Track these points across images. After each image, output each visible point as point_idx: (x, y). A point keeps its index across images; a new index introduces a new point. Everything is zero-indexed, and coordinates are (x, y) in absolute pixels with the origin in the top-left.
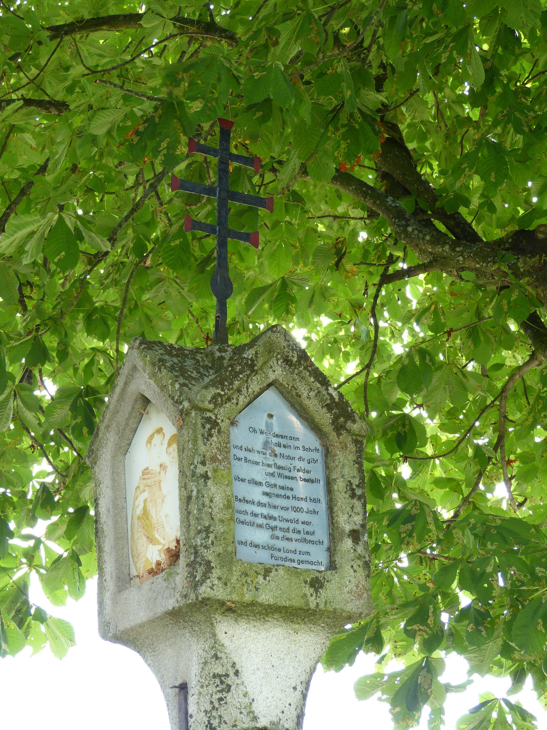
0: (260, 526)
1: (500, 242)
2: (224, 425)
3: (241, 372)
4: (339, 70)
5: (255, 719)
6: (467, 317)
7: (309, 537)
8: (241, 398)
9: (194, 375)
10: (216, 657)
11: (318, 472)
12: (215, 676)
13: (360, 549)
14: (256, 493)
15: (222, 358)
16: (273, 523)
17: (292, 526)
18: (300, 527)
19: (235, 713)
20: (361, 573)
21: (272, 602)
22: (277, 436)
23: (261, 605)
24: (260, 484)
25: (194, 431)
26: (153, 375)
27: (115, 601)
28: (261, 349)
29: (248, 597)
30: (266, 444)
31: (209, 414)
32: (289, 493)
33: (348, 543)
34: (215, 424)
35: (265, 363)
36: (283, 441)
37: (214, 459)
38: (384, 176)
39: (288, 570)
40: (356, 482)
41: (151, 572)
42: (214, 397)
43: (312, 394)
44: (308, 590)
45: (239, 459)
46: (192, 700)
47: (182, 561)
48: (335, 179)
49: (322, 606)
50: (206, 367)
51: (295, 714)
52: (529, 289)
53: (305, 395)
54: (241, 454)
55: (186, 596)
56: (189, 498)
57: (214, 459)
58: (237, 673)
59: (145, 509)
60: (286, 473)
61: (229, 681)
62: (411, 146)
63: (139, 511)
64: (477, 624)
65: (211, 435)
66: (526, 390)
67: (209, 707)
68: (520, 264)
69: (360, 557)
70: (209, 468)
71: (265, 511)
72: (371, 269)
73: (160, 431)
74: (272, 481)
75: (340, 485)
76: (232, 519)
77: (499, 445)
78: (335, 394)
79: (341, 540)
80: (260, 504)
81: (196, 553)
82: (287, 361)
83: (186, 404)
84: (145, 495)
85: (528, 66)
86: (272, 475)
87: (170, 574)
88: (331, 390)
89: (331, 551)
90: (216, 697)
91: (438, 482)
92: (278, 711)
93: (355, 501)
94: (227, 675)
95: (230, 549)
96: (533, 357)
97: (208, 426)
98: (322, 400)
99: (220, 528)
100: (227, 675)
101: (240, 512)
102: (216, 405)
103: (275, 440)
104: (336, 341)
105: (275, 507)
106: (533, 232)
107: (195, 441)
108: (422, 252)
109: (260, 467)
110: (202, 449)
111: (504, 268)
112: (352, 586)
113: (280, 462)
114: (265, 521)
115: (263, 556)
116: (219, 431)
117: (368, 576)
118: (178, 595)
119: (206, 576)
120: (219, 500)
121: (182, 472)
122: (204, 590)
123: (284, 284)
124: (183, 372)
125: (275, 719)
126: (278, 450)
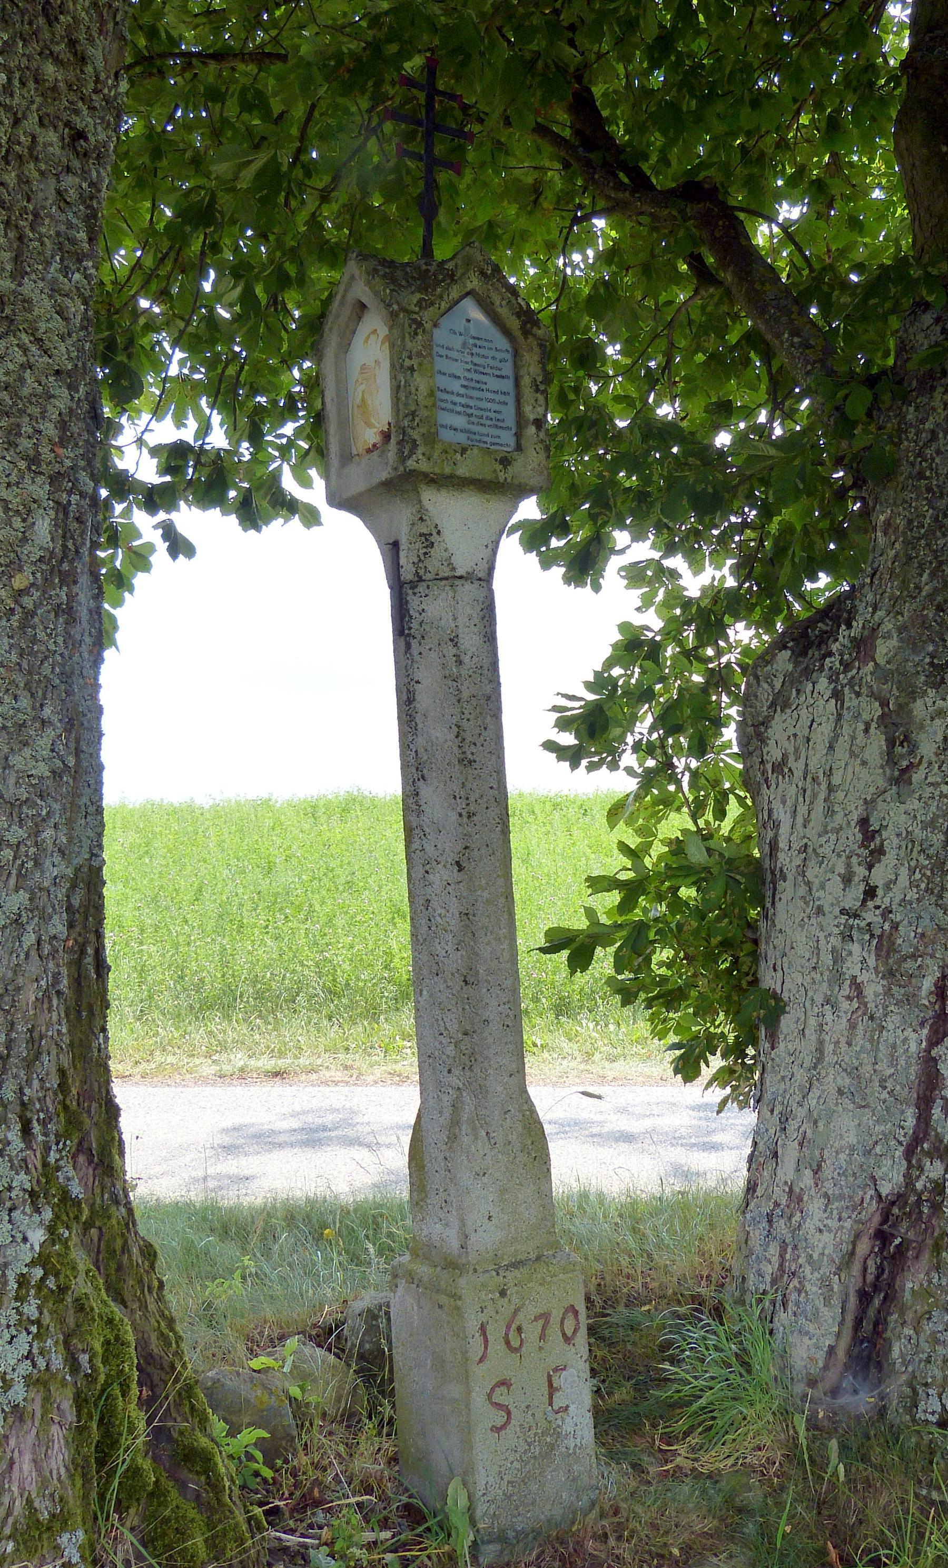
0: (459, 413)
1: (672, 191)
2: (428, 326)
3: (443, 281)
4: (535, 22)
5: (454, 569)
6: (643, 256)
7: (500, 424)
8: (443, 304)
9: (404, 283)
10: (421, 519)
11: (508, 369)
12: (421, 535)
13: (542, 435)
14: (455, 386)
15: (427, 271)
16: (469, 411)
17: (485, 414)
18: (492, 415)
19: (438, 564)
20: (543, 455)
21: (468, 475)
22: (474, 338)
23: (459, 477)
24: (459, 378)
25: (403, 330)
26: (368, 283)
27: (339, 475)
28: (460, 262)
29: (447, 471)
30: (464, 344)
31: (415, 316)
32: (484, 387)
33: (532, 429)
34: (420, 324)
35: (464, 274)
36: (479, 343)
37: (419, 354)
38: (577, 132)
39: (481, 449)
40: (540, 379)
41: (369, 451)
42: (420, 302)
43: (504, 303)
44: (499, 467)
45: (441, 356)
46: (402, 554)
47: (393, 440)
48: (534, 130)
49: (509, 480)
50: (413, 278)
51: (486, 566)
52: (694, 230)
53: (498, 303)
54: (443, 352)
55: (396, 469)
56: (398, 387)
57: (419, 354)
58: (439, 533)
59: (363, 399)
60: (481, 370)
61: (432, 539)
62: (605, 113)
63: (358, 401)
64: (640, 501)
65: (416, 334)
66: (690, 322)
67: (416, 560)
68: (688, 210)
69: (542, 441)
70: (415, 362)
71: (463, 401)
72: (564, 214)
73: (374, 332)
74: (469, 376)
75: (526, 381)
76: (434, 405)
77: (667, 366)
78: (523, 303)
79: (526, 427)
80: (458, 395)
81: (404, 433)
82: (483, 273)
83: (395, 307)
84: (363, 386)
85: (704, 45)
86: (469, 370)
87: (383, 451)
88: (520, 300)
89: (518, 436)
90: (422, 551)
91: (617, 399)
92: (473, 564)
93: (538, 395)
94: (431, 535)
95: (432, 430)
96: (696, 291)
97: (414, 326)
98: (512, 309)
99: (424, 413)
100: (431, 535)
101: (442, 401)
102: (421, 308)
103: (472, 341)
104: (540, 287)
105: (471, 398)
106: (699, 183)
107: (403, 339)
108: (608, 198)
109: (459, 363)
110: (409, 345)
111: (675, 213)
112: (535, 465)
113: (476, 360)
114: (463, 409)
115: (461, 438)
116: (424, 331)
117: (548, 457)
118: (389, 469)
119: (412, 452)
120: (423, 389)
121: (392, 366)
122: (411, 464)
123: (490, 224)
124: (393, 280)
125: (470, 570)
126: (475, 350)
